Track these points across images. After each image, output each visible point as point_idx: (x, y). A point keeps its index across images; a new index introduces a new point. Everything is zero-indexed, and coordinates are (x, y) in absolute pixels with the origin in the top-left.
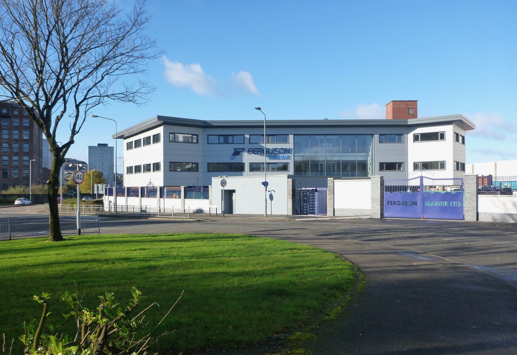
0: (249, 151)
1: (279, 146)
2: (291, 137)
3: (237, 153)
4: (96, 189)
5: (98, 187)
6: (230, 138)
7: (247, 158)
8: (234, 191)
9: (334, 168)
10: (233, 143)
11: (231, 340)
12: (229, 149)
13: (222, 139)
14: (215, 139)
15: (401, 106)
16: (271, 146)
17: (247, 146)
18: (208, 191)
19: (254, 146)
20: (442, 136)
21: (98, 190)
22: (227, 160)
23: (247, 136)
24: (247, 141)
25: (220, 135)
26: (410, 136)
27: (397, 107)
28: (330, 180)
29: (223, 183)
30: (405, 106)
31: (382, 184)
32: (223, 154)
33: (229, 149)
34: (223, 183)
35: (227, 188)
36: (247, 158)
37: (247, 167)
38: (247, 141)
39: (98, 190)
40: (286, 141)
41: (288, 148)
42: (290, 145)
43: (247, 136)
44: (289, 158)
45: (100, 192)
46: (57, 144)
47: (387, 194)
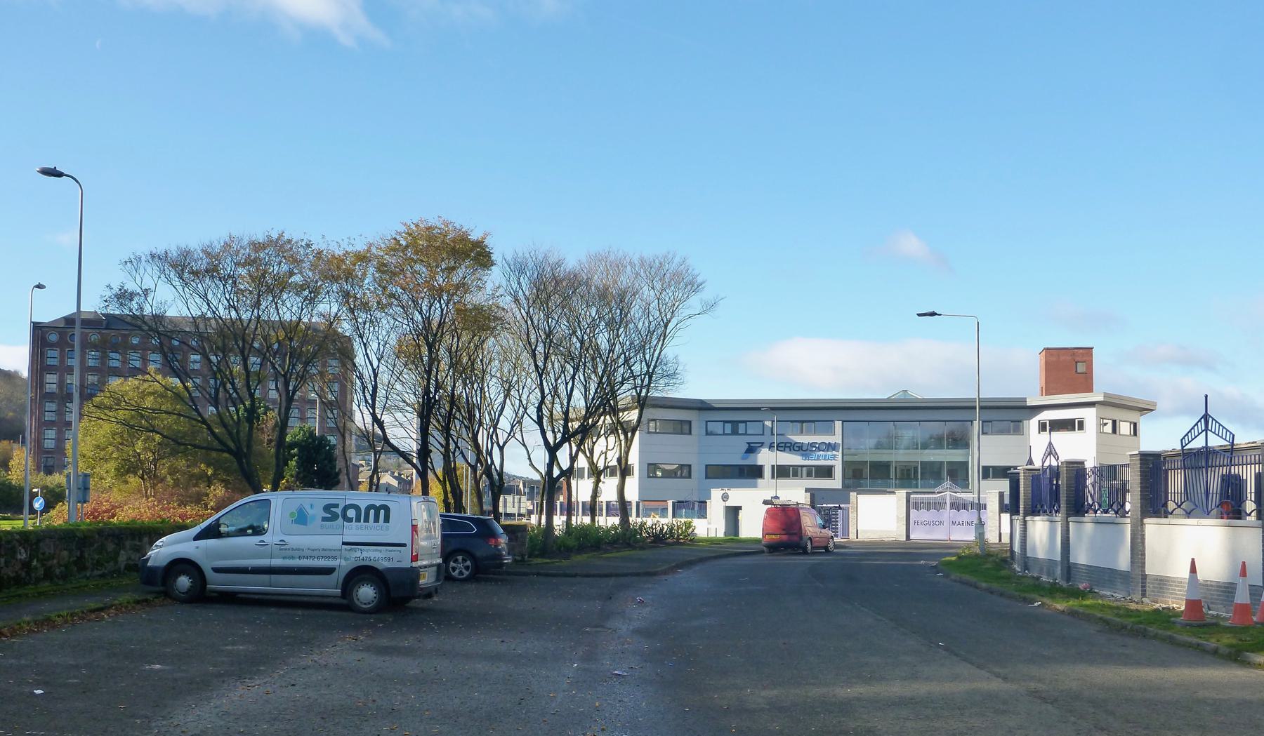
0: (771, 447)
1: (818, 439)
2: (838, 424)
3: (751, 449)
4: (501, 504)
5: (505, 501)
6: (742, 426)
7: (766, 458)
8: (740, 508)
9: (916, 472)
10: (746, 434)
11: (603, 295)
12: (741, 443)
13: (728, 428)
14: (718, 427)
15: (1062, 358)
16: (805, 439)
17: (767, 439)
18: (706, 508)
19: (781, 439)
20: (1081, 425)
21: (505, 506)
22: (736, 459)
23: (768, 423)
24: (768, 432)
25: (725, 422)
26: (1033, 423)
27: (1054, 359)
28: (853, 494)
29: (725, 497)
30: (1069, 358)
31: (908, 501)
32: (732, 453)
33: (741, 443)
34: (725, 497)
35: (729, 503)
36: (766, 458)
37: (767, 472)
38: (768, 432)
39: (505, 506)
40: (831, 431)
41: (833, 442)
42: (836, 438)
43: (768, 423)
44: (834, 458)
45: (509, 511)
46: (167, 314)
47: (913, 512)
